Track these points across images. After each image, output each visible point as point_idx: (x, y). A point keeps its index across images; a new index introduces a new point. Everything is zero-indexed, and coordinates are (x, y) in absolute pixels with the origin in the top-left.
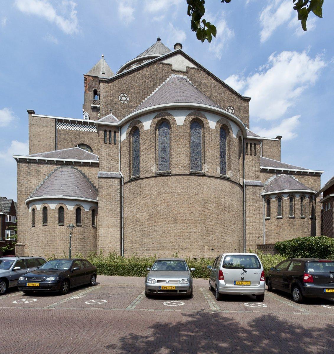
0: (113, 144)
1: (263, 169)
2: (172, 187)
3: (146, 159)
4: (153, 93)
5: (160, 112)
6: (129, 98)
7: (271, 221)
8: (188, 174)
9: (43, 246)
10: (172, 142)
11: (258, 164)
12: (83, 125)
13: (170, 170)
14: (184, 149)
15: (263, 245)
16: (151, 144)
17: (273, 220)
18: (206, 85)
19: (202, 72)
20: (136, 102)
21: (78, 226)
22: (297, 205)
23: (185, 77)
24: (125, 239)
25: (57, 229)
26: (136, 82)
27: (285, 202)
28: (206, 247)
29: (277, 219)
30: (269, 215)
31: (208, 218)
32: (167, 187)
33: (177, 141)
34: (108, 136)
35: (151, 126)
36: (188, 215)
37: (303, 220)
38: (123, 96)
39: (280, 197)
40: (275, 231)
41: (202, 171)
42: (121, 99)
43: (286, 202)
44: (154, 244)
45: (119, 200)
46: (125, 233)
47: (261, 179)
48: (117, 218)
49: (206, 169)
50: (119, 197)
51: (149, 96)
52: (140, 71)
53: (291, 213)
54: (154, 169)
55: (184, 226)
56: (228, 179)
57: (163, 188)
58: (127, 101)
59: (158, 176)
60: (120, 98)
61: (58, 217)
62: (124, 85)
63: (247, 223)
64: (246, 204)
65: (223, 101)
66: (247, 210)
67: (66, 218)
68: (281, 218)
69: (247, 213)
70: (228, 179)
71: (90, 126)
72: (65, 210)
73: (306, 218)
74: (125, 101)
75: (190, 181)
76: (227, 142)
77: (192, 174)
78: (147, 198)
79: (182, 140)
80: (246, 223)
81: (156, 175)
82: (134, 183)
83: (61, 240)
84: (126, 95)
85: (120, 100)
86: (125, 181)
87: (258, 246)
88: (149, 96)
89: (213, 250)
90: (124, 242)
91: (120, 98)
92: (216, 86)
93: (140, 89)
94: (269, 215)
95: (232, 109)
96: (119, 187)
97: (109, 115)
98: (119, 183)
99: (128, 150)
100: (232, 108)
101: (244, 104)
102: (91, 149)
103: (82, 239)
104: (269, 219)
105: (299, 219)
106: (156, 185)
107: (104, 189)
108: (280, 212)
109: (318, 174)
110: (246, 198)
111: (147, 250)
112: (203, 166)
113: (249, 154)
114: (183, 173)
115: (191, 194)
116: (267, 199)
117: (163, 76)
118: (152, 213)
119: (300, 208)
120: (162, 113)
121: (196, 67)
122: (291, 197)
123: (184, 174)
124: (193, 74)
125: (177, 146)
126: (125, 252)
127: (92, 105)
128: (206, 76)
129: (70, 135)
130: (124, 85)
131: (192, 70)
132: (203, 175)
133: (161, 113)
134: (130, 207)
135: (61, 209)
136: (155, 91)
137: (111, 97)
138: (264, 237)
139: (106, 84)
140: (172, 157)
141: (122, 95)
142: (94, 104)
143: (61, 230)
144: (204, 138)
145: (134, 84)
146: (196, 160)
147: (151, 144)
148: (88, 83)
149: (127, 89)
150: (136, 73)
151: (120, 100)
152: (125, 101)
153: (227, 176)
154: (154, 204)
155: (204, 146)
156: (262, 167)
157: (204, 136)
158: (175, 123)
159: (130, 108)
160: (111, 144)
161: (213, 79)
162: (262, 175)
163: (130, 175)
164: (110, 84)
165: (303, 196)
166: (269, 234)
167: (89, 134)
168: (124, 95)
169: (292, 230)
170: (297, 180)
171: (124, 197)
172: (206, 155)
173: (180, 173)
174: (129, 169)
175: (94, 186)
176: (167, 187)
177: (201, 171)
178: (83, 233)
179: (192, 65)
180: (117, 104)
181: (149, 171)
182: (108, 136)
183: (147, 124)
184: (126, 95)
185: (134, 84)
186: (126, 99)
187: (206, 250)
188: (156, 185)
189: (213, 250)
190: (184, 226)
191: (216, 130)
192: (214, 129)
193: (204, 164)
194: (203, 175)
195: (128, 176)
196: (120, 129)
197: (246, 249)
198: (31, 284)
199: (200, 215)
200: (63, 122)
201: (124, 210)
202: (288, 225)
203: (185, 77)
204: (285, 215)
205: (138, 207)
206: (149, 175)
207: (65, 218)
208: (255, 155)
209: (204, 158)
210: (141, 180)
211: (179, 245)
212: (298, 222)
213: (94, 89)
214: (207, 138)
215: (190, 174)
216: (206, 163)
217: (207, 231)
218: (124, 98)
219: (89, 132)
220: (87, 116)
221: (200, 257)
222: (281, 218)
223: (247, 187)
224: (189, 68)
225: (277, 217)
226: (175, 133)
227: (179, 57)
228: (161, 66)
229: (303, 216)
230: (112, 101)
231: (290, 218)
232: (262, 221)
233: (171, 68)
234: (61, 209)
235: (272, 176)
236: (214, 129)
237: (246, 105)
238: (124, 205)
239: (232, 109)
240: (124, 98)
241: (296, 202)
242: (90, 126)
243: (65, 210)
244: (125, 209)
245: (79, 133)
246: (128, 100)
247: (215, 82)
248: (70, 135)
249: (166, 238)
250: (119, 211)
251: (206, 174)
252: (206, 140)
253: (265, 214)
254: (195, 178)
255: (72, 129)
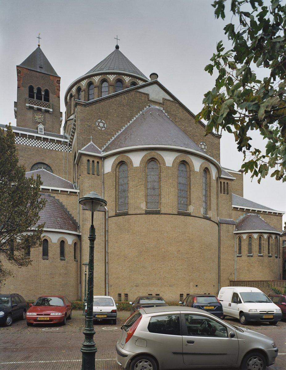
0: (96, 175)
1: (234, 208)
2: (161, 226)
3: (135, 196)
4: (131, 122)
5: (150, 151)
6: (107, 125)
7: (243, 258)
8: (176, 213)
9: (25, 281)
10: (162, 182)
11: (231, 203)
12: (43, 142)
13: (159, 209)
14: (172, 190)
15: (235, 281)
16: (140, 182)
17: (244, 258)
18: (181, 119)
19: (177, 105)
20: (114, 130)
21: (61, 260)
22: (265, 245)
23: (162, 109)
24: (110, 274)
25: (41, 263)
26: (114, 109)
27: (255, 241)
28: (192, 284)
29: (248, 256)
30: (240, 253)
31: (193, 256)
32: (157, 225)
33: (166, 181)
34: (91, 167)
35: (140, 164)
36: (175, 253)
37: (270, 258)
38: (100, 122)
39: (250, 236)
40: (246, 268)
41: (188, 211)
42: (99, 125)
43: (256, 241)
44: (143, 281)
45: (103, 234)
46: (109, 268)
47: (233, 217)
48: (101, 253)
49: (191, 209)
50: (104, 231)
51: (127, 124)
52: (118, 98)
53: (260, 252)
54: (143, 206)
55: (173, 264)
56: (209, 219)
57: (152, 226)
58: (105, 128)
59: (147, 213)
60: (97, 124)
61: (42, 250)
62: (101, 111)
63: (221, 260)
64: (220, 241)
65: (197, 136)
66: (221, 247)
67: (50, 251)
68: (252, 256)
69: (221, 250)
70: (209, 219)
71: (50, 143)
72: (49, 243)
73: (273, 256)
74: (103, 127)
75: (178, 221)
76: (208, 184)
77: (179, 214)
78: (137, 235)
79: (170, 181)
80: (220, 259)
81: (146, 212)
82: (121, 217)
83: (45, 275)
84: (103, 122)
85: (98, 126)
86: (110, 215)
87: (231, 283)
88: (127, 124)
89: (197, 286)
90: (109, 277)
91: (97, 124)
92: (190, 120)
93: (117, 116)
94: (240, 253)
95: (204, 145)
96: (104, 221)
97: (89, 144)
98: (104, 216)
99: (115, 184)
100: (205, 144)
101: (215, 140)
102: (50, 168)
103: (66, 274)
104: (241, 256)
105: (267, 258)
106: (146, 223)
107: (88, 222)
108: (250, 251)
109: (280, 215)
110: (220, 235)
111: (136, 286)
112: (189, 207)
113: (223, 192)
114: (171, 213)
115: (179, 233)
116: (238, 237)
117: (140, 105)
118: (141, 250)
119: (267, 246)
120: (152, 153)
121: (172, 99)
122: (260, 237)
123: (173, 213)
124: (169, 107)
125: (166, 186)
126: (109, 288)
127: (28, 105)
128: (181, 110)
129: (28, 151)
130: (101, 111)
131: (168, 103)
132: (189, 215)
133: (151, 152)
134: (117, 243)
135: (62, 243)
136: (133, 120)
137: (88, 122)
138: (236, 273)
139: (83, 108)
140: (162, 197)
141: (99, 121)
142: (29, 103)
143: (46, 264)
144: (190, 180)
145: (111, 111)
146: (182, 200)
147: (140, 182)
148: (21, 77)
149: (104, 115)
150: (113, 100)
151: (98, 126)
152: (103, 127)
153: (208, 216)
154: (143, 241)
155: (190, 188)
156: (233, 206)
157: (190, 178)
158: (164, 164)
159: (108, 135)
160: (89, 174)
161: (187, 114)
162: (234, 212)
163: (116, 210)
164: (87, 108)
165: (270, 236)
166: (241, 271)
167: (49, 152)
168: (101, 121)
169: (261, 267)
170: (263, 219)
171: (109, 231)
172: (192, 196)
173: (169, 213)
174: (115, 203)
175: (72, 216)
176: (157, 225)
177: (187, 211)
178: (66, 267)
179: (168, 97)
180: (94, 130)
181: (138, 208)
182: (91, 167)
183: (136, 160)
184: (103, 122)
185: (111, 111)
186: (104, 126)
187: (191, 286)
188: (146, 223)
189: (197, 286)
190: (173, 264)
191: (200, 173)
192: (199, 171)
193: (190, 205)
194: (189, 215)
195: (114, 210)
196: (104, 160)
197: (220, 285)
198: (267, 317)
199: (186, 254)
200: (19, 136)
201: (109, 244)
202: (258, 262)
203: (162, 109)
204: (255, 253)
205: (126, 243)
206: (138, 212)
207: (49, 252)
208: (228, 194)
209: (190, 199)
210: (129, 216)
211: (167, 282)
212: (266, 259)
213: (29, 85)
214: (193, 180)
215: (178, 214)
216: (192, 204)
217: (193, 268)
218: (101, 125)
219: (49, 150)
220: (42, 129)
221: (186, 293)
222: (252, 256)
223: (221, 224)
224: (164, 99)
225: (248, 254)
226: (164, 174)
227: (156, 87)
228: (138, 95)
229: (270, 255)
230: (89, 126)
231: (259, 256)
232: (234, 258)
233: (148, 98)
234: (62, 243)
235: (243, 215)
236: (199, 171)
237: (217, 142)
238: (109, 239)
239: (204, 145)
240: (101, 125)
241: (264, 242)
242: (50, 143)
243: (49, 243)
244: (110, 244)
245: (38, 150)
246: (97, 123)
247: (190, 116)
248: (28, 151)
249: (155, 275)
250: (104, 245)
251: (211, 219)
252: (192, 182)
253: (236, 252)
254: (182, 217)
255: (29, 145)
